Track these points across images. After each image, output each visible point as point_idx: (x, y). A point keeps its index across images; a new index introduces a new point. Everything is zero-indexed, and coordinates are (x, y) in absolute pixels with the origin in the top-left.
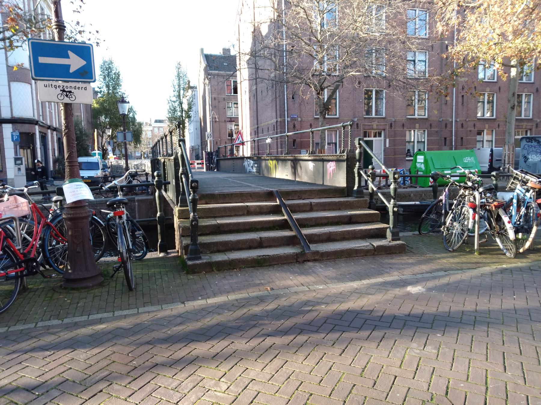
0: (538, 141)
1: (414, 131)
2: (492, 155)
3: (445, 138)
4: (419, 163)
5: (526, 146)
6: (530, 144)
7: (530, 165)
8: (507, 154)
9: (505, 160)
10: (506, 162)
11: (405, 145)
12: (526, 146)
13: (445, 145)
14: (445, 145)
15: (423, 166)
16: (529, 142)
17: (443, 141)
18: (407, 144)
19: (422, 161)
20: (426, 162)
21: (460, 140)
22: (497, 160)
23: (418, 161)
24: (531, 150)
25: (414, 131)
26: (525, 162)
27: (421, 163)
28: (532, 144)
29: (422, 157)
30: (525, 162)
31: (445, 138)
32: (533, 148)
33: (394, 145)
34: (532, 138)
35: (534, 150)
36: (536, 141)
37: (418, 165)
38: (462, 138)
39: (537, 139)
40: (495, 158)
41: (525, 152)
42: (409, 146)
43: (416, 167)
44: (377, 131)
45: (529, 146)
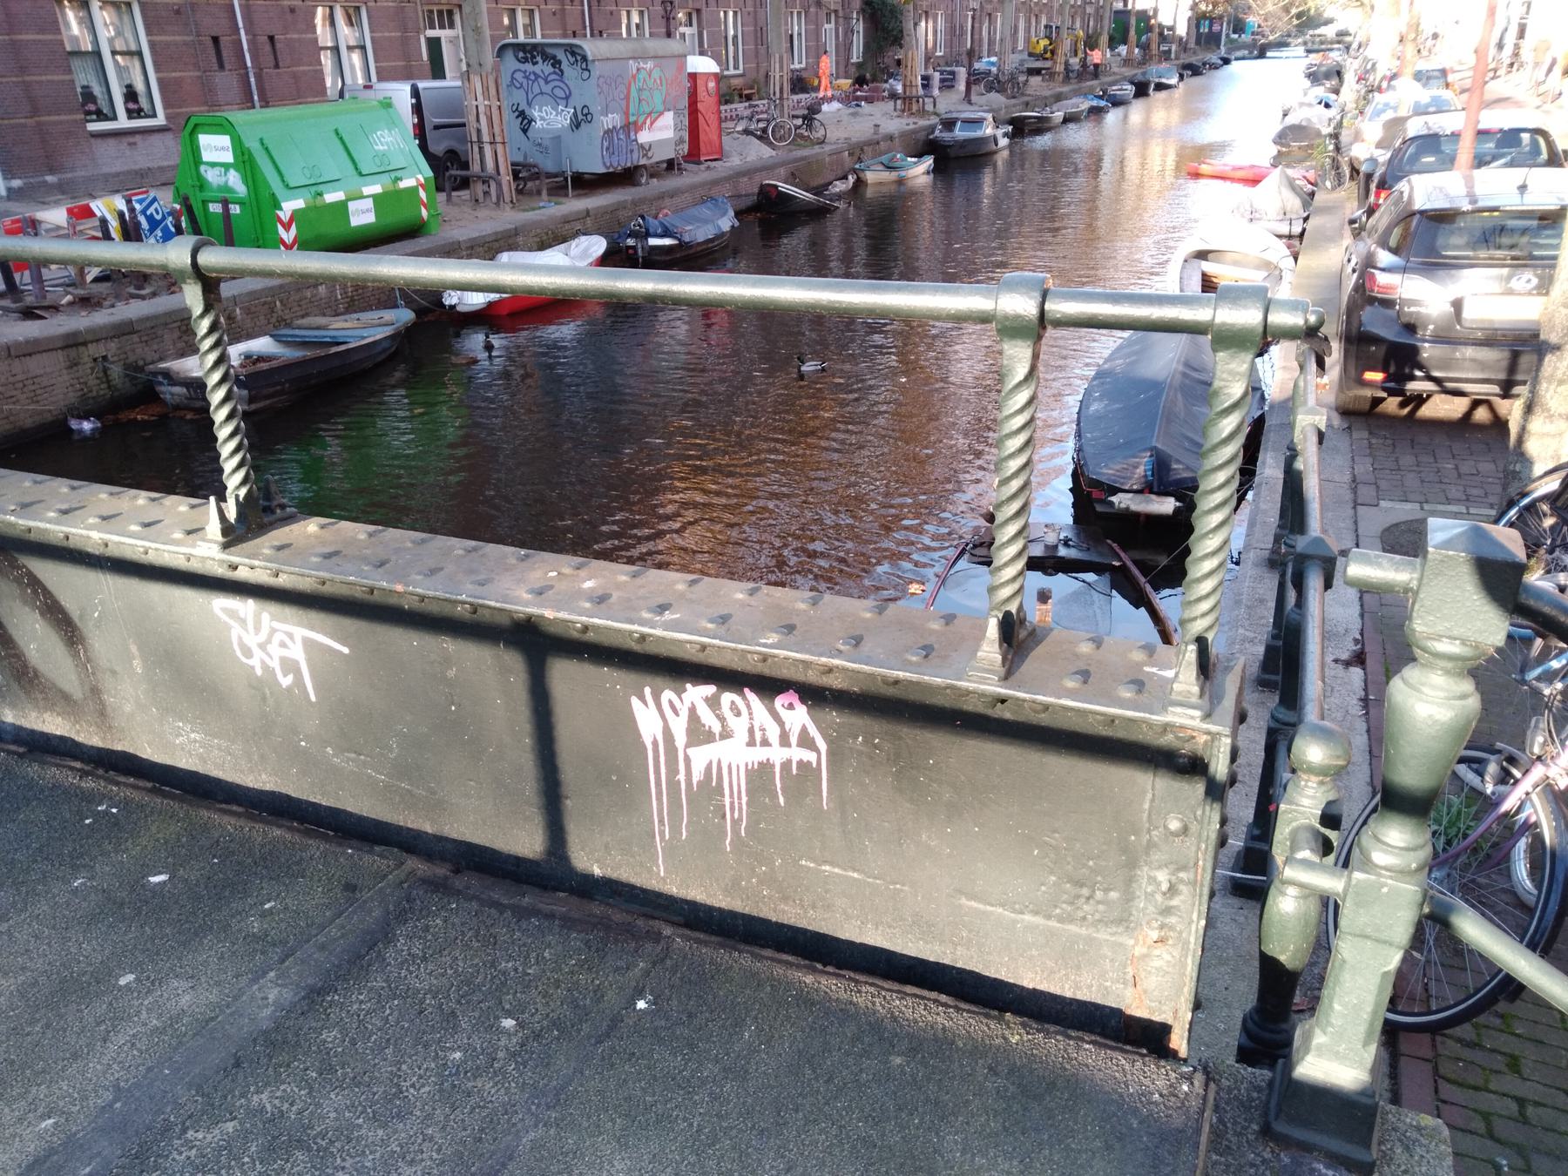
0: (554, 57)
1: (628, 13)
2: (418, 109)
3: (216, 40)
4: (213, 165)
5: (519, 76)
6: (528, 67)
7: (546, 143)
8: (481, 109)
9: (479, 131)
10: (486, 138)
11: (69, 71)
12: (519, 76)
13: (221, 66)
14: (221, 66)
15: (234, 180)
16: (525, 60)
17: (212, 52)
18: (76, 64)
19: (228, 157)
20: (244, 161)
21: (268, 48)
22: (437, 127)
23: (207, 156)
24: (536, 90)
25: (628, 13)
26: (525, 131)
27: (226, 166)
28: (537, 69)
29: (225, 140)
30: (525, 131)
31: (216, 40)
32: (542, 82)
33: (23, 70)
34: (535, 46)
35: (547, 89)
36: (546, 57)
37: (212, 176)
38: (271, 38)
39: (550, 51)
40: (431, 120)
41: (519, 97)
42: (84, 76)
43: (202, 185)
44: (445, 8)
45: (527, 78)
